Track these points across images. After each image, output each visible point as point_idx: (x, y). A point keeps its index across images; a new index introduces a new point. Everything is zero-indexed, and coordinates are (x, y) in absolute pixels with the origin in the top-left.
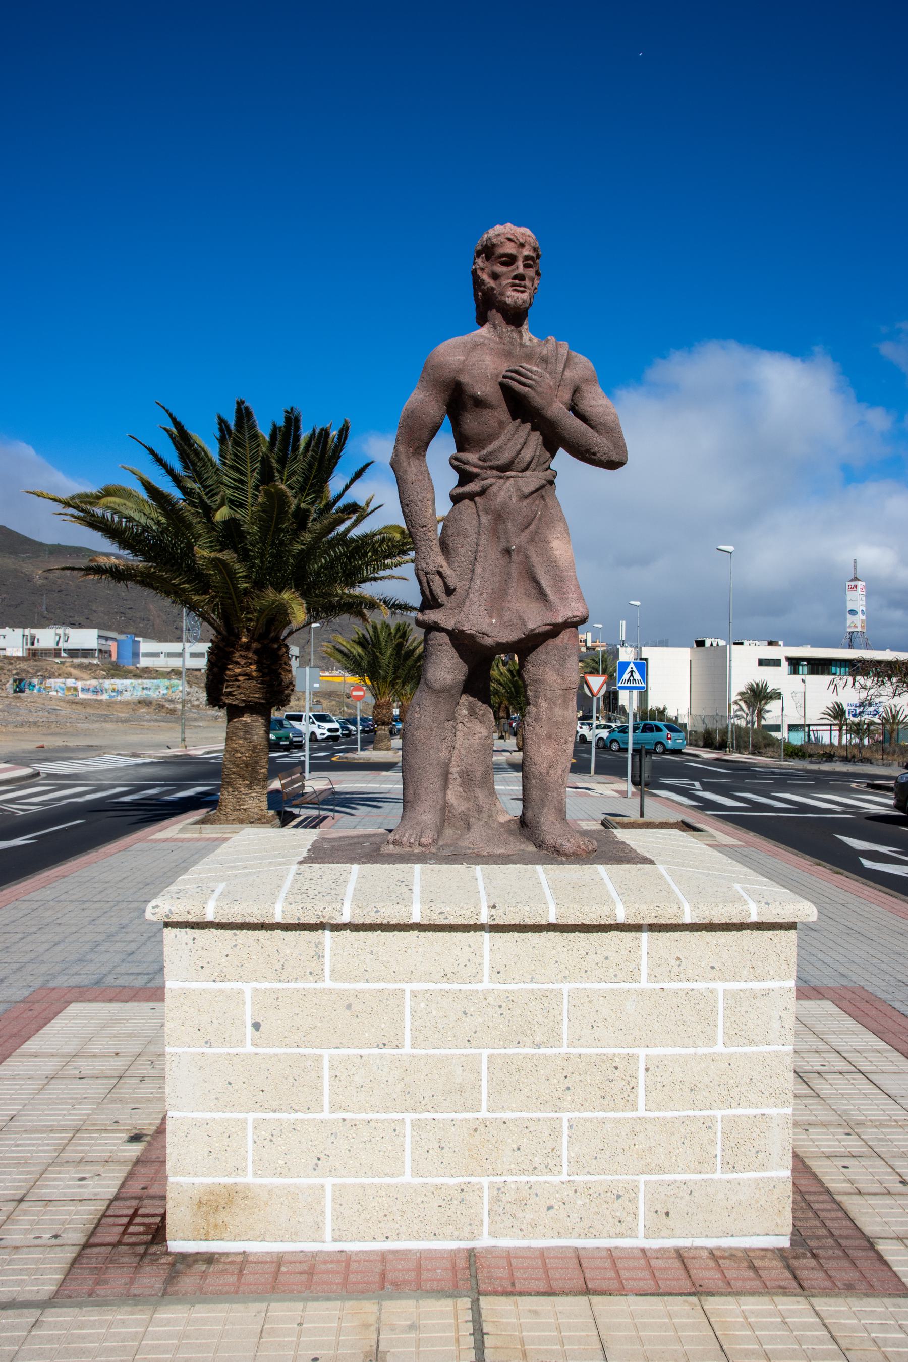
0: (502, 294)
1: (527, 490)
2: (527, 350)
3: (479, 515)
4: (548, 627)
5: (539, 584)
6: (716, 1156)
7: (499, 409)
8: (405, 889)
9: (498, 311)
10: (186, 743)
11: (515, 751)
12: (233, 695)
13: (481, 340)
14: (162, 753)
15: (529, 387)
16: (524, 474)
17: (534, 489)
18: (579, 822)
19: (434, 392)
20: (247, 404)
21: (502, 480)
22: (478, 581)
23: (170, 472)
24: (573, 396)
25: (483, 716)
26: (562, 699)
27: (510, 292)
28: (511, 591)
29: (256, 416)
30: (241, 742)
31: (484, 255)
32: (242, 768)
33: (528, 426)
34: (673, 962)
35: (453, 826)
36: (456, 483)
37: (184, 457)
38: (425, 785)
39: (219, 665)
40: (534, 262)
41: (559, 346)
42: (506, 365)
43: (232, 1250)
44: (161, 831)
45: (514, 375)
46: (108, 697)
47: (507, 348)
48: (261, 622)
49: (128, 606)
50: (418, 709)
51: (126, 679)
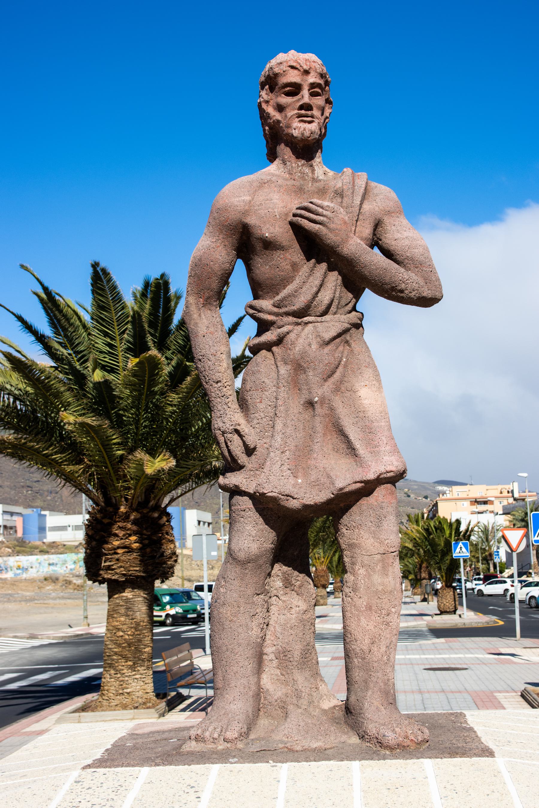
0: (289, 126)
1: (327, 336)
2: (320, 185)
3: (277, 367)
4: (359, 485)
5: (347, 437)
8: (193, 796)
9: (287, 145)
10: (89, 621)
11: (436, 615)
13: (269, 178)
14: (63, 633)
15: (320, 224)
16: (324, 318)
17: (335, 334)
18: (496, 694)
19: (221, 236)
20: (103, 265)
21: (300, 326)
22: (278, 438)
23: (41, 339)
24: (375, 230)
25: (300, 587)
26: (380, 564)
27: (296, 123)
28: (316, 447)
30: (122, 619)
31: (267, 87)
32: (124, 648)
33: (324, 266)
35: (269, 715)
36: (256, 333)
37: (54, 323)
38: (235, 669)
39: (97, 538)
40: (323, 89)
41: (356, 178)
42: (296, 202)
44: (38, 721)
45: (303, 212)
46: (13, 576)
47: (297, 183)
48: (138, 491)
49: (35, 479)
50: (223, 583)
51: (32, 555)
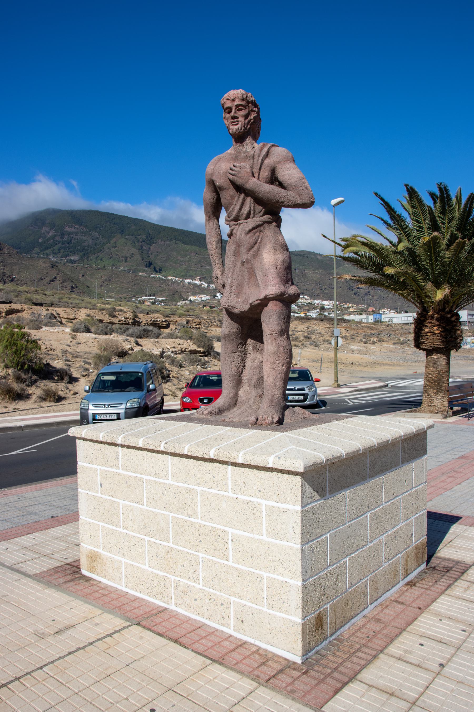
4: (259, 301)
6: (264, 598)
7: (229, 190)
12: (425, 344)
29: (417, 189)
30: (431, 369)
32: (432, 383)
34: (241, 484)
37: (392, 218)
43: (98, 580)
46: (470, 347)
